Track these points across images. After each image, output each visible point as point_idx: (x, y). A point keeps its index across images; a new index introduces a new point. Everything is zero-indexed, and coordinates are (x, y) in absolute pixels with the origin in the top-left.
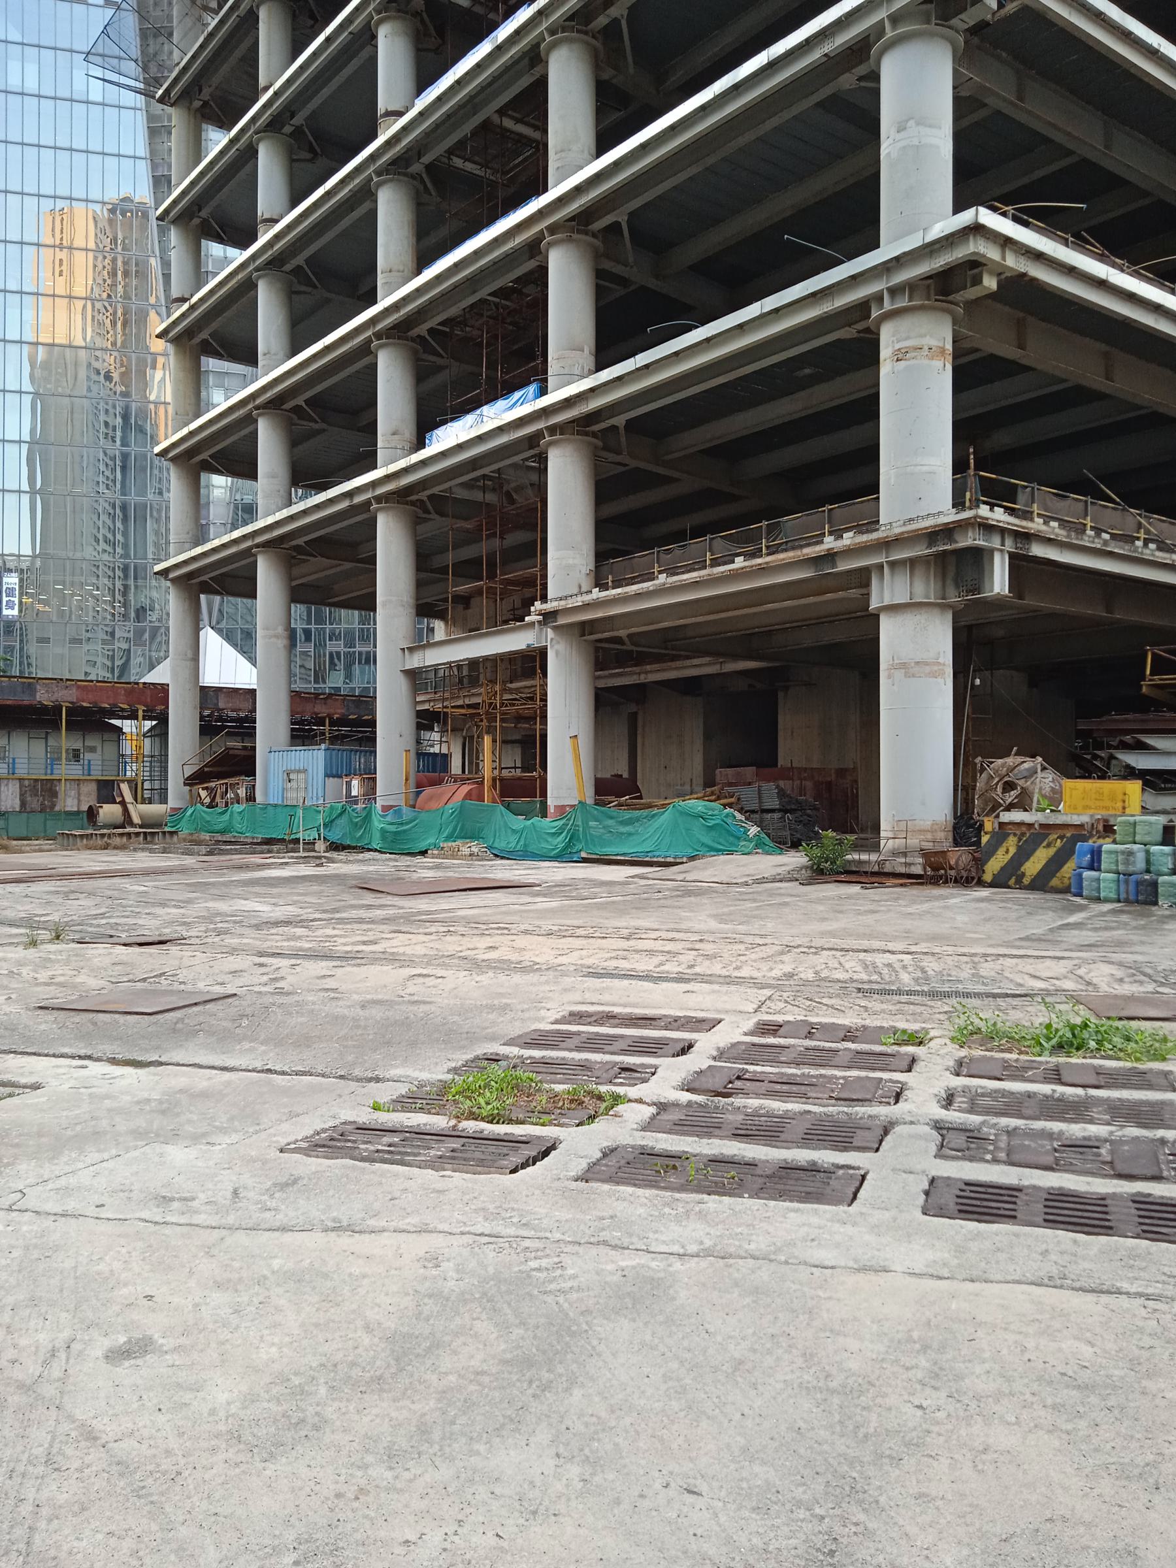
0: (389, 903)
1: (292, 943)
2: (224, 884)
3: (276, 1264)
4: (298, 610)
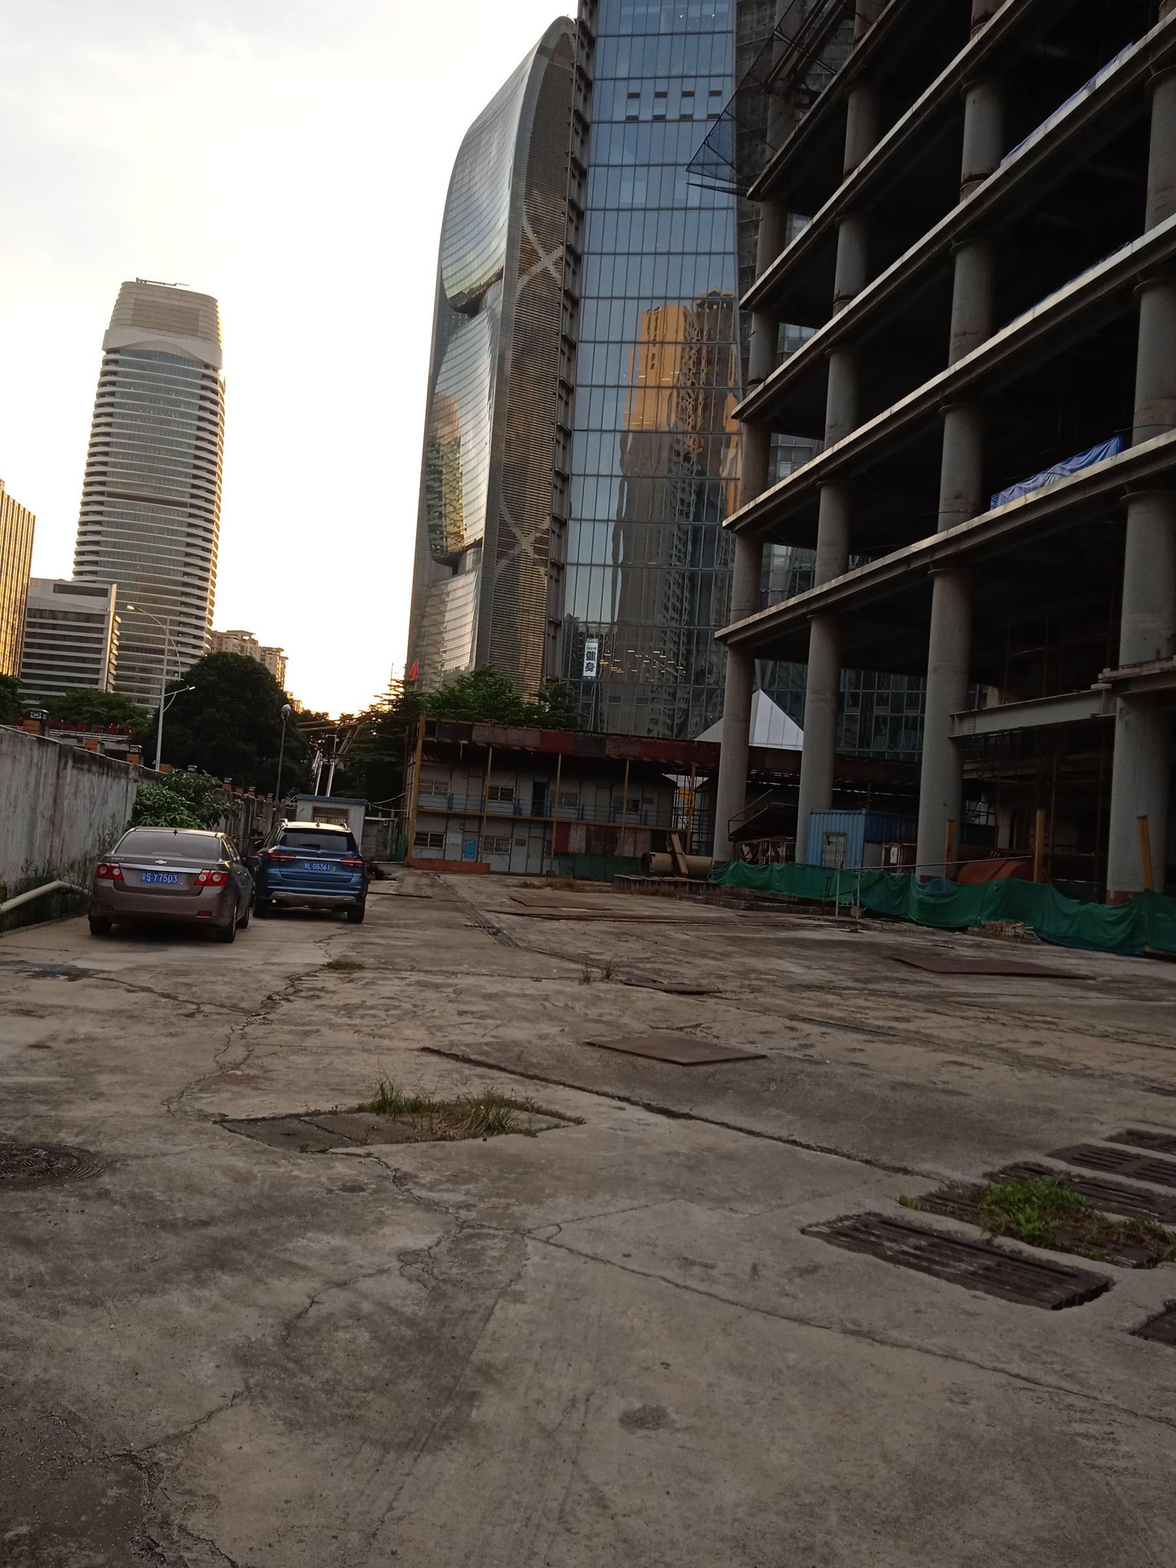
0: (925, 979)
1: (823, 1010)
2: (761, 941)
3: (792, 1357)
4: (847, 675)
